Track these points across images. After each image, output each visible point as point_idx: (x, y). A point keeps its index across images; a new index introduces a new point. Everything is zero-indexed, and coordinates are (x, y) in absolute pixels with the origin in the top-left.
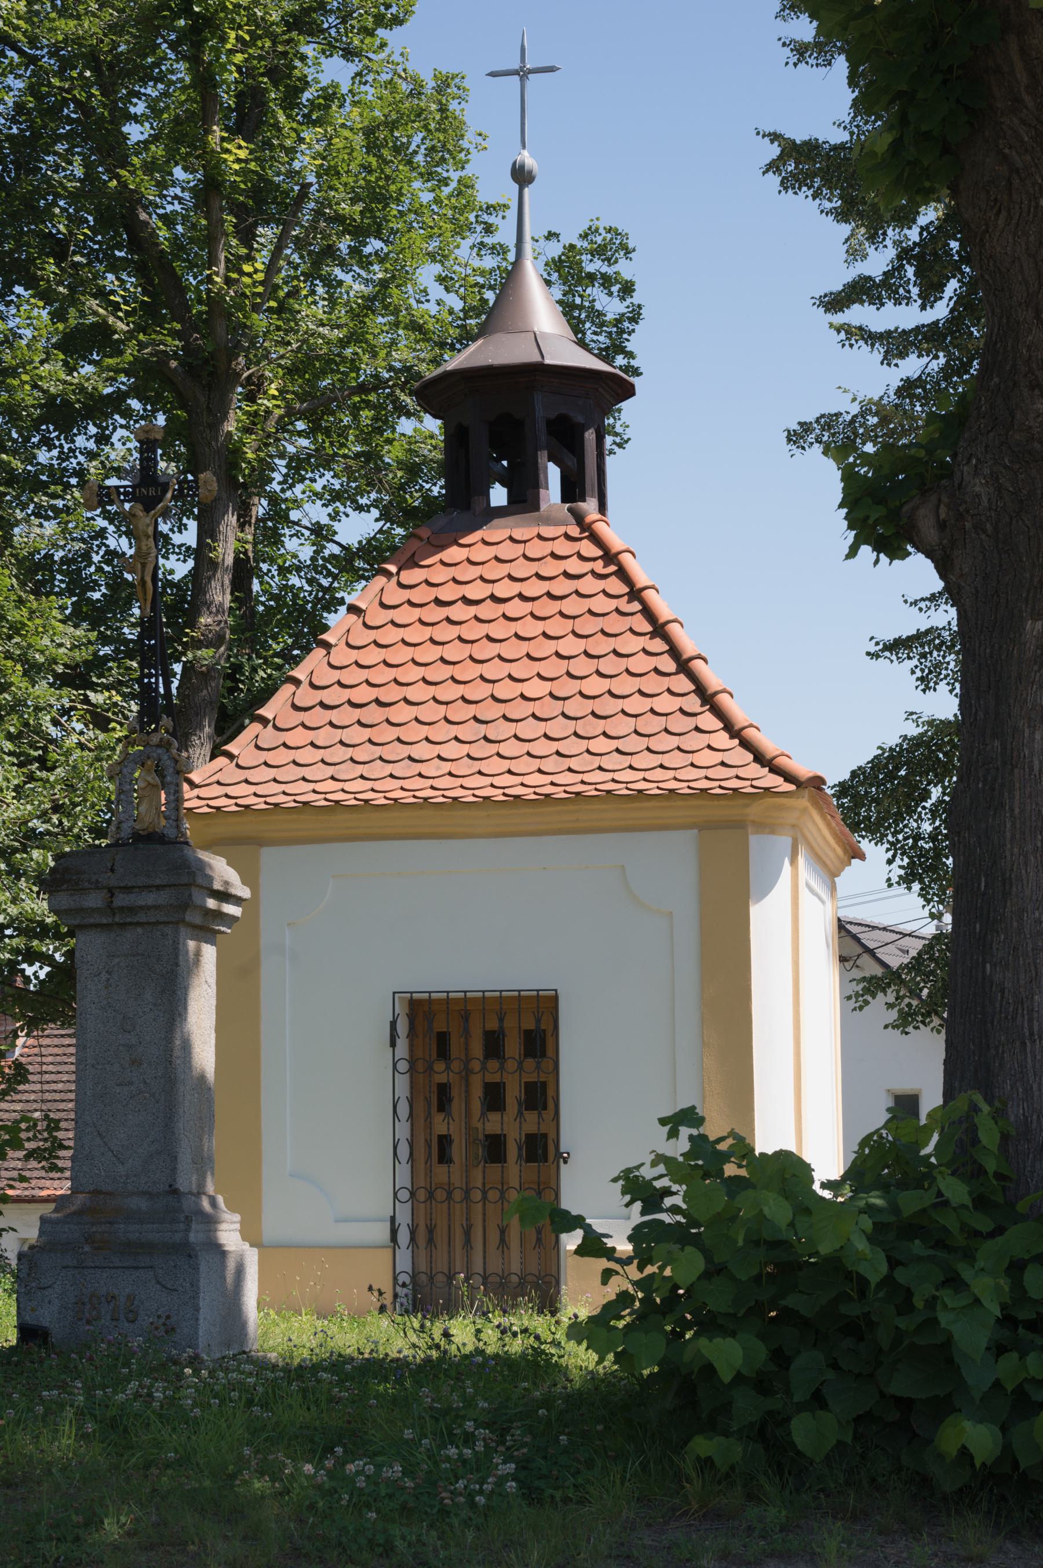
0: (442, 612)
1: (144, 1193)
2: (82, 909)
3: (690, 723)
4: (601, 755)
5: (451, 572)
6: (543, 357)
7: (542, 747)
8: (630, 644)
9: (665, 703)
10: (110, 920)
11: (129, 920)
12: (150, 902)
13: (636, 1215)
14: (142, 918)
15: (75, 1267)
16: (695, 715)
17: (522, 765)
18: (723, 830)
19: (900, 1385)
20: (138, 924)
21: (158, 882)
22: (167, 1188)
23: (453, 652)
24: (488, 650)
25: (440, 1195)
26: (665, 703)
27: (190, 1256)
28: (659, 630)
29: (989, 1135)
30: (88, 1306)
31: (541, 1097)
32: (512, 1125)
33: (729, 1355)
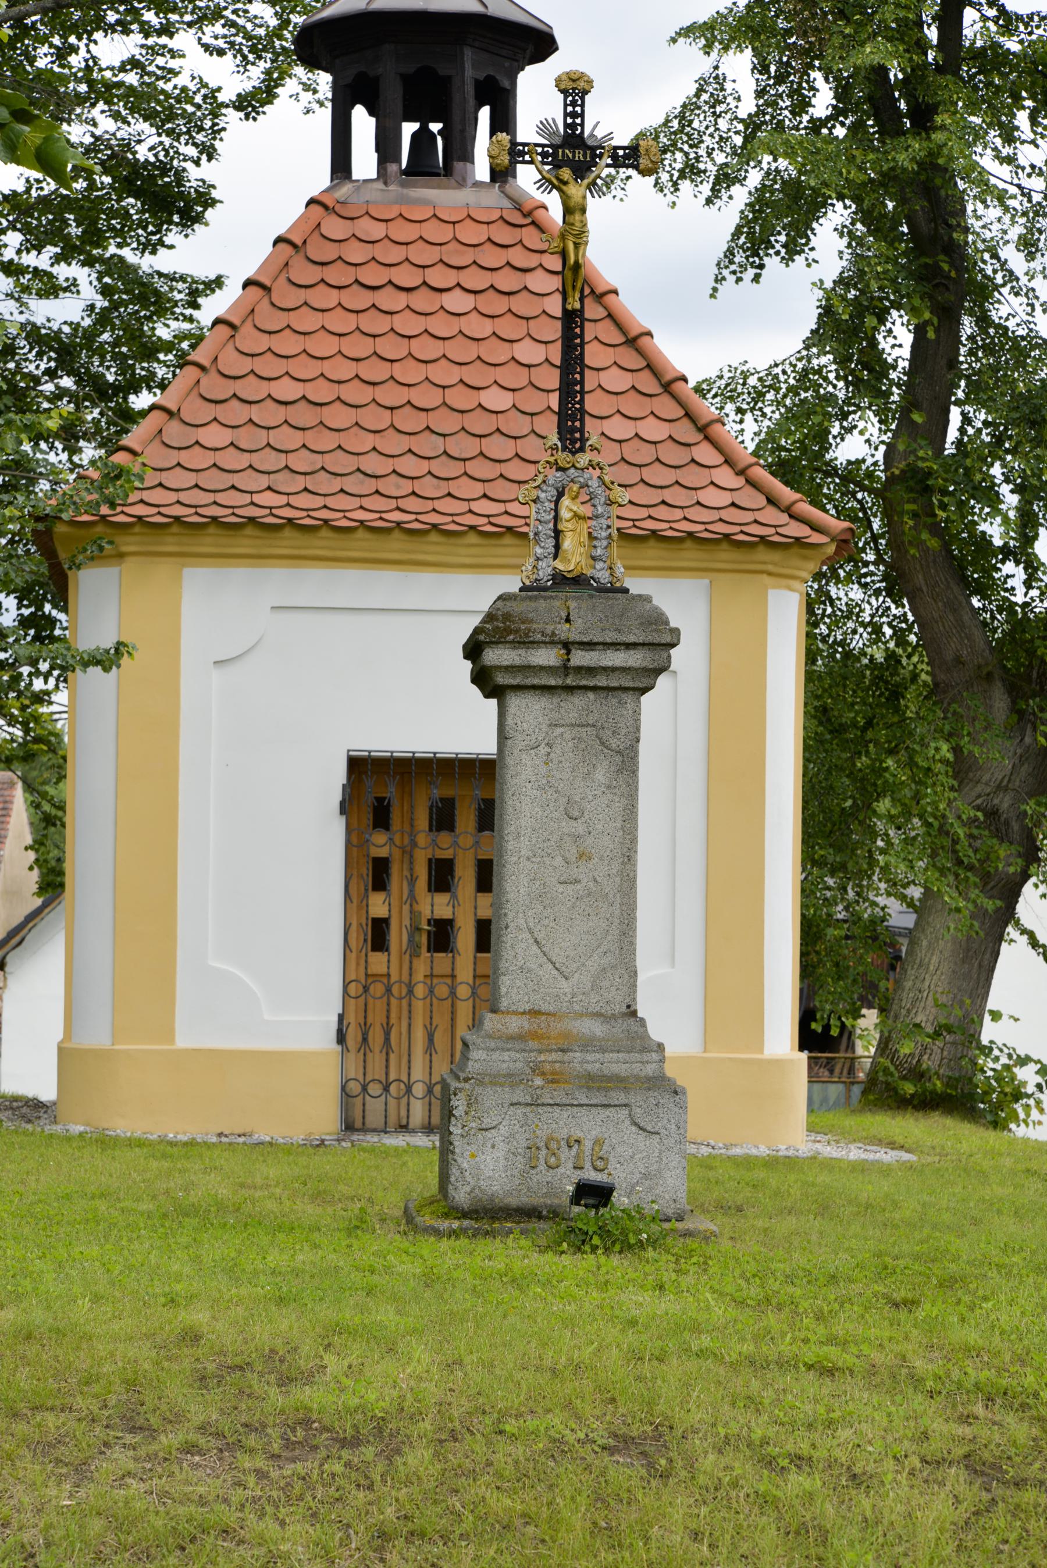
1: (598, 1015)
2: (529, 667)
6: (486, 7)
11: (584, 682)
14: (602, 681)
15: (527, 1105)
16: (688, 445)
20: (594, 689)
21: (632, 639)
22: (624, 1009)
23: (389, 347)
25: (377, 989)
27: (676, 1092)
32: (462, 907)
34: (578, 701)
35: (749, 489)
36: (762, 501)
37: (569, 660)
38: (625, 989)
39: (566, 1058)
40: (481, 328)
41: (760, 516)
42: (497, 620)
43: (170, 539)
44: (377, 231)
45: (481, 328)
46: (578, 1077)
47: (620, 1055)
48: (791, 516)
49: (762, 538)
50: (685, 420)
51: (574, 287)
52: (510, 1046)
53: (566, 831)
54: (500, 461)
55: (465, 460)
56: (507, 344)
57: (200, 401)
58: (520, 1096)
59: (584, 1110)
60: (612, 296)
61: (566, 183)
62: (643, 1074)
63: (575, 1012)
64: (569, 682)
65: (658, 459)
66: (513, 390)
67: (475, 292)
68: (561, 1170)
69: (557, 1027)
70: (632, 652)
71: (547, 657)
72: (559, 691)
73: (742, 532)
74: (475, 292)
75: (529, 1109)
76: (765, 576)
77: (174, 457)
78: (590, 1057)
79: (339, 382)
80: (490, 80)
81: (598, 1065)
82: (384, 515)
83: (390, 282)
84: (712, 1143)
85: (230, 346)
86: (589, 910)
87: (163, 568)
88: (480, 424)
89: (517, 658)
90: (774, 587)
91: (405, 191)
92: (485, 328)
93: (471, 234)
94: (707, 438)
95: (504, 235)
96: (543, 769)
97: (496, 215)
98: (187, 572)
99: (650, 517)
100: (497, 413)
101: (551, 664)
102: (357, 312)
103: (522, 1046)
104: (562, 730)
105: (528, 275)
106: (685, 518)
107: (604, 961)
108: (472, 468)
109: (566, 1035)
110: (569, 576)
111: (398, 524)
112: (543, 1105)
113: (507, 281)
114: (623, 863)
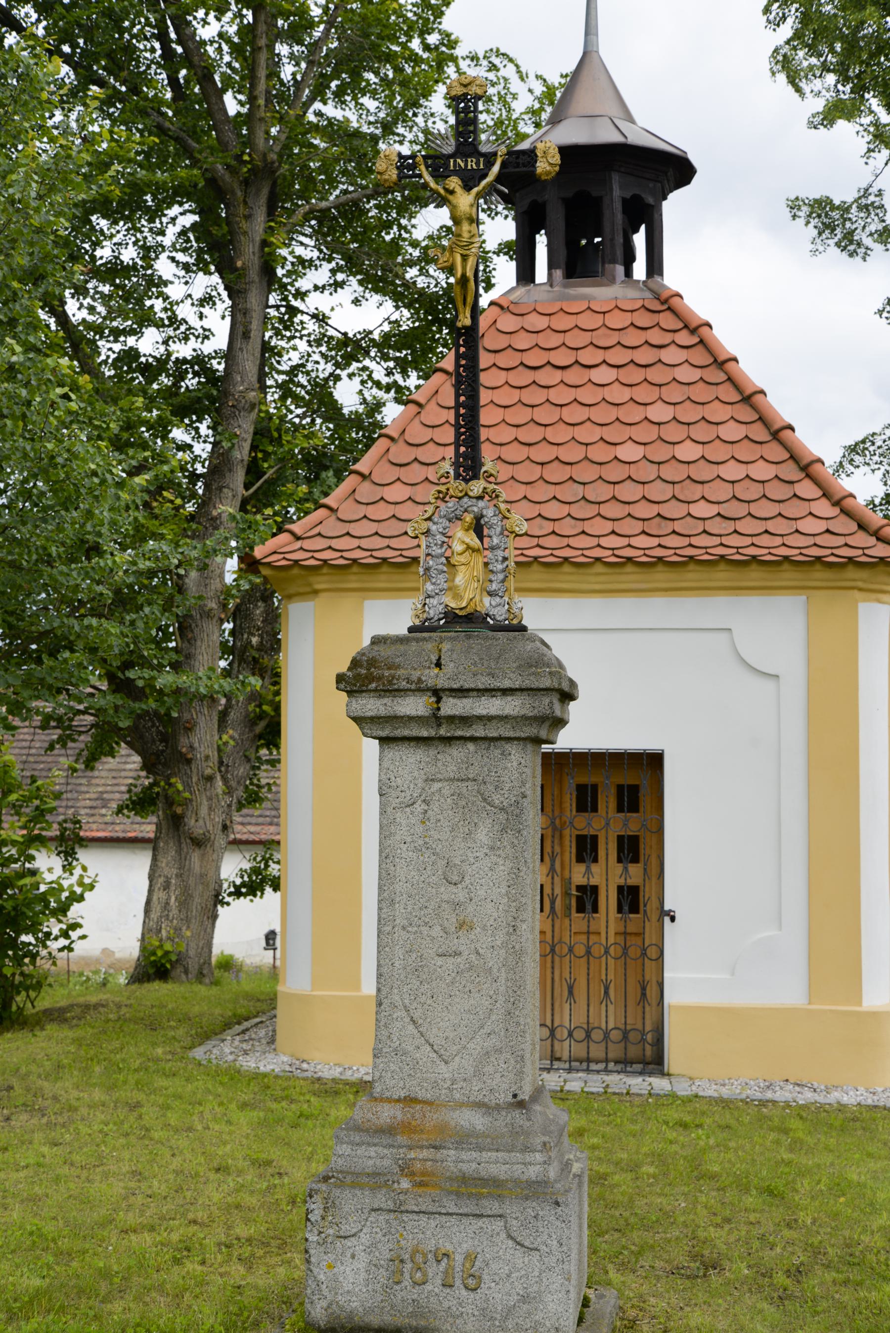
2: (396, 717)
4: (673, 520)
8: (718, 412)
10: (433, 733)
11: (459, 733)
12: (493, 711)
15: (390, 1211)
16: (791, 482)
20: (473, 739)
21: (507, 684)
22: (510, 1099)
23: (544, 415)
26: (762, 471)
27: (557, 1204)
30: (409, 1266)
34: (457, 753)
35: (843, 518)
36: (854, 526)
37: (439, 709)
38: (511, 1075)
39: (439, 1156)
40: (619, 394)
41: (850, 541)
42: (361, 666)
43: (353, 577)
44: (541, 323)
45: (619, 394)
46: (450, 1179)
47: (500, 1154)
48: (878, 539)
49: (850, 559)
50: (791, 462)
51: (465, 304)
52: (376, 1141)
53: (445, 897)
54: (629, 503)
55: (599, 503)
56: (642, 407)
57: (389, 465)
58: (381, 1200)
59: (453, 1219)
60: (733, 363)
61: (452, 192)
62: (524, 1178)
63: (454, 1100)
64: (442, 732)
65: (764, 496)
66: (645, 444)
67: (618, 367)
68: (428, 1287)
69: (433, 1118)
70: (509, 698)
71: (415, 706)
72: (436, 743)
73: (833, 554)
74: (618, 367)
75: (392, 1216)
76: (856, 591)
77: (362, 511)
78: (465, 1156)
79: (501, 445)
80: (636, 198)
81: (474, 1165)
82: (525, 552)
83: (549, 362)
84: (816, 1085)
85: (417, 421)
86: (470, 986)
87: (348, 602)
88: (615, 473)
89: (382, 708)
90: (864, 601)
91: (567, 290)
92: (624, 395)
93: (617, 320)
94: (808, 476)
95: (643, 319)
96: (419, 829)
97: (639, 304)
98: (368, 604)
99: (753, 544)
100: (630, 463)
101: (420, 713)
102: (520, 388)
103: (390, 1141)
104: (440, 785)
105: (663, 351)
106: (784, 545)
107: (489, 1044)
108: (605, 510)
109: (442, 1128)
110: (460, 613)
111: (536, 558)
112: (407, 1212)
113: (644, 356)
114: (508, 934)
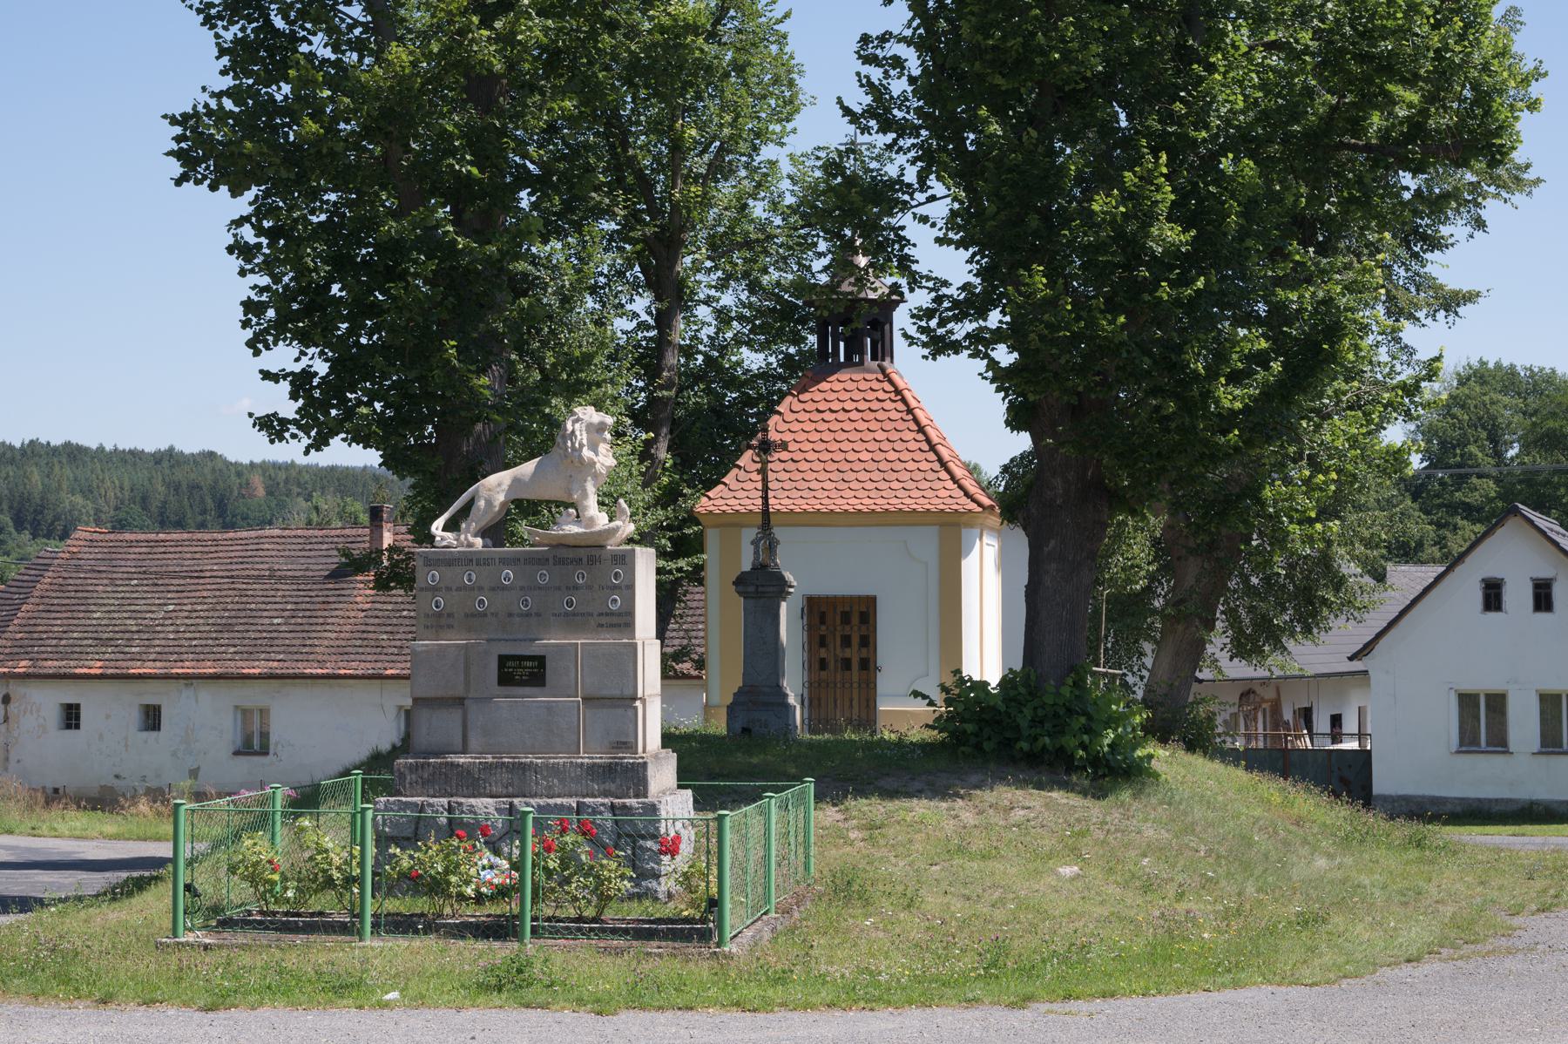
0: (820, 416)
3: (935, 476)
5: (823, 395)
7: (869, 485)
9: (924, 466)
13: (944, 695)
17: (861, 494)
18: (950, 532)
19: (1008, 735)
24: (843, 436)
26: (924, 466)
28: (921, 430)
29: (1033, 677)
31: (868, 641)
32: (854, 653)
33: (970, 728)
